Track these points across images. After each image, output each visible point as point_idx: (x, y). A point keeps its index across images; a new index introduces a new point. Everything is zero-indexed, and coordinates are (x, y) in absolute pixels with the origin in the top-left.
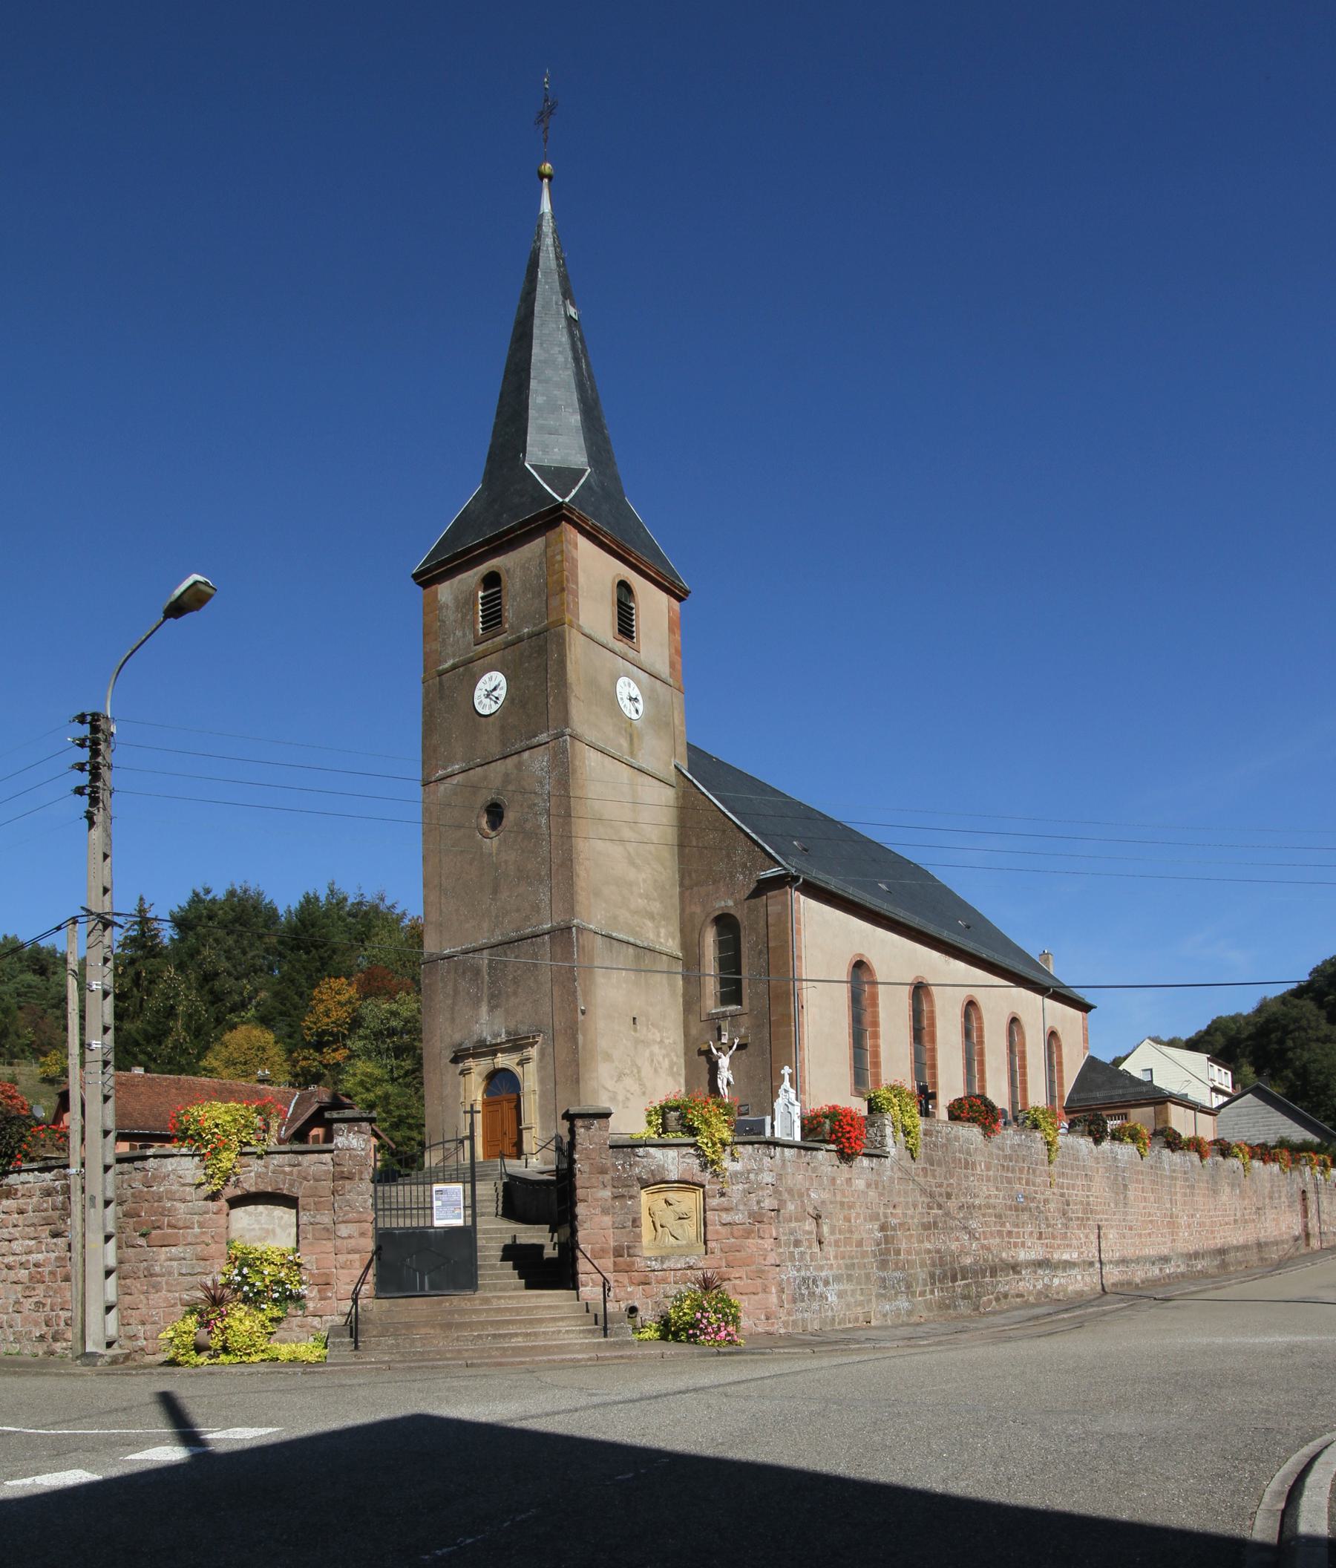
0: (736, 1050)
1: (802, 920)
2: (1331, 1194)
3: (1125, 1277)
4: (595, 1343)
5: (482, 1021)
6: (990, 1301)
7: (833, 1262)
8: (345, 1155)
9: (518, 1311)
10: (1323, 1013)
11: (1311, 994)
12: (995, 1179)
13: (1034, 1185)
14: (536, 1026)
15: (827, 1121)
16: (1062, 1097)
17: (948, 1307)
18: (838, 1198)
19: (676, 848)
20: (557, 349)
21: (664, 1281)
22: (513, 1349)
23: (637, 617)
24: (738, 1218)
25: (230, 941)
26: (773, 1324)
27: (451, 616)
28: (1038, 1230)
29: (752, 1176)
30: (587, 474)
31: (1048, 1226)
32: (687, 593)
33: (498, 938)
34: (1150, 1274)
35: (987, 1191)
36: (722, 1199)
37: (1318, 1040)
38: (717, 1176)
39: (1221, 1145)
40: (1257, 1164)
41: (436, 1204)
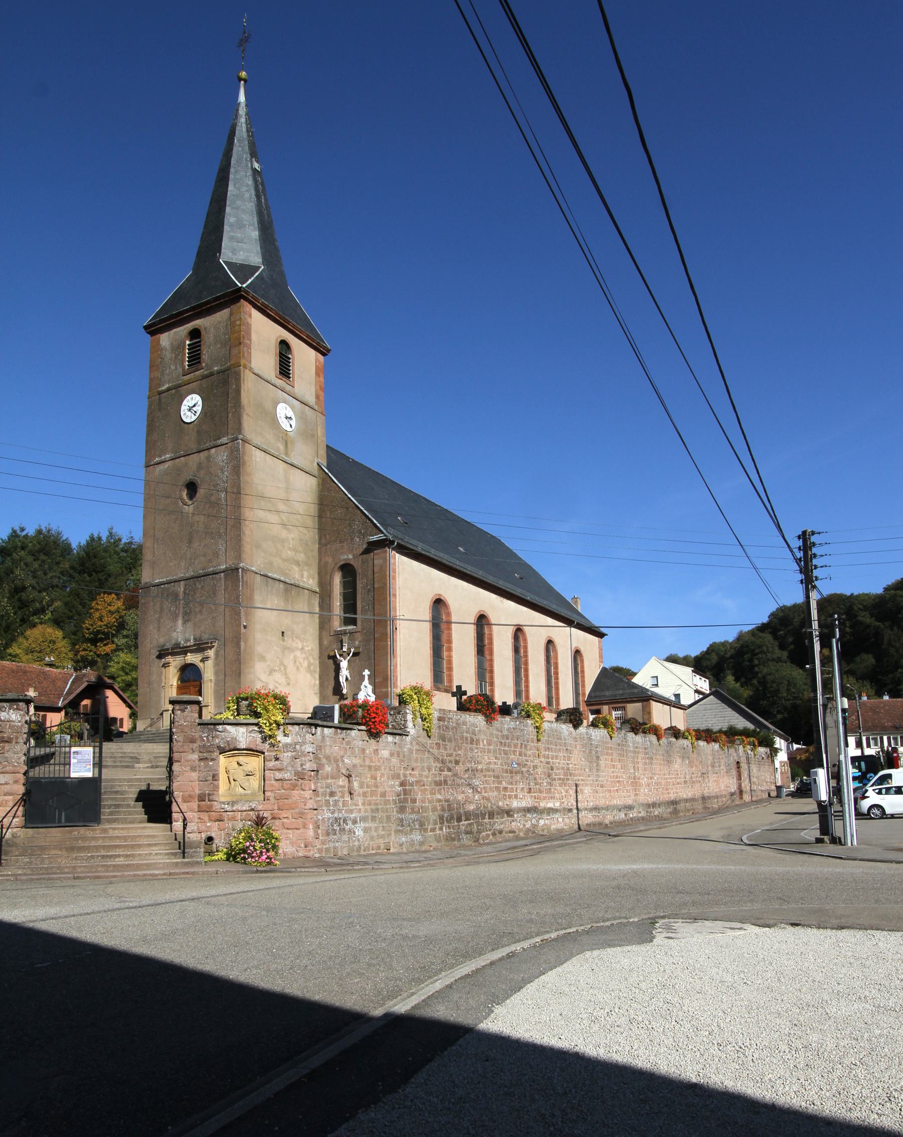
0: (352, 656)
1: (397, 570)
2: (760, 765)
3: (597, 819)
4: (174, 863)
5: (178, 630)
6: (488, 836)
7: (361, 807)
8: (6, 725)
9: (125, 838)
10: (777, 643)
11: (769, 630)
12: (495, 751)
13: (525, 755)
14: (214, 635)
15: (360, 710)
16: (584, 694)
17: (454, 839)
18: (367, 763)
19: (317, 518)
20: (245, 189)
21: (233, 819)
22: (114, 866)
23: (293, 364)
24: (287, 776)
25: (36, 565)
26: (310, 850)
27: (168, 355)
28: (528, 787)
29: (298, 747)
30: (261, 270)
31: (536, 784)
32: (329, 351)
33: (191, 573)
34: (617, 818)
35: (487, 759)
36: (277, 762)
37: (773, 660)
38: (274, 746)
39: (674, 730)
40: (702, 743)
41: (73, 761)
